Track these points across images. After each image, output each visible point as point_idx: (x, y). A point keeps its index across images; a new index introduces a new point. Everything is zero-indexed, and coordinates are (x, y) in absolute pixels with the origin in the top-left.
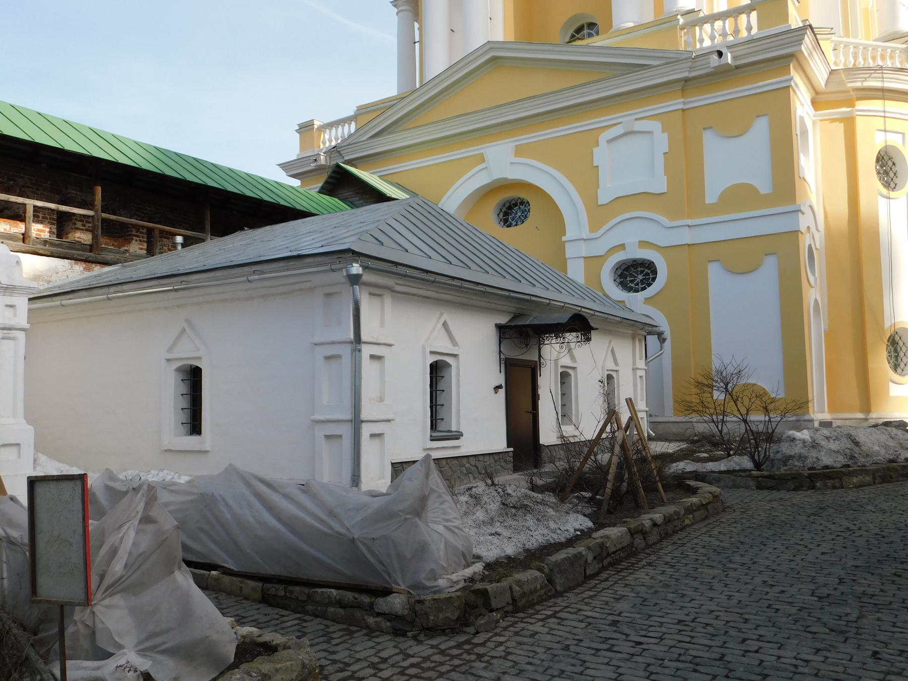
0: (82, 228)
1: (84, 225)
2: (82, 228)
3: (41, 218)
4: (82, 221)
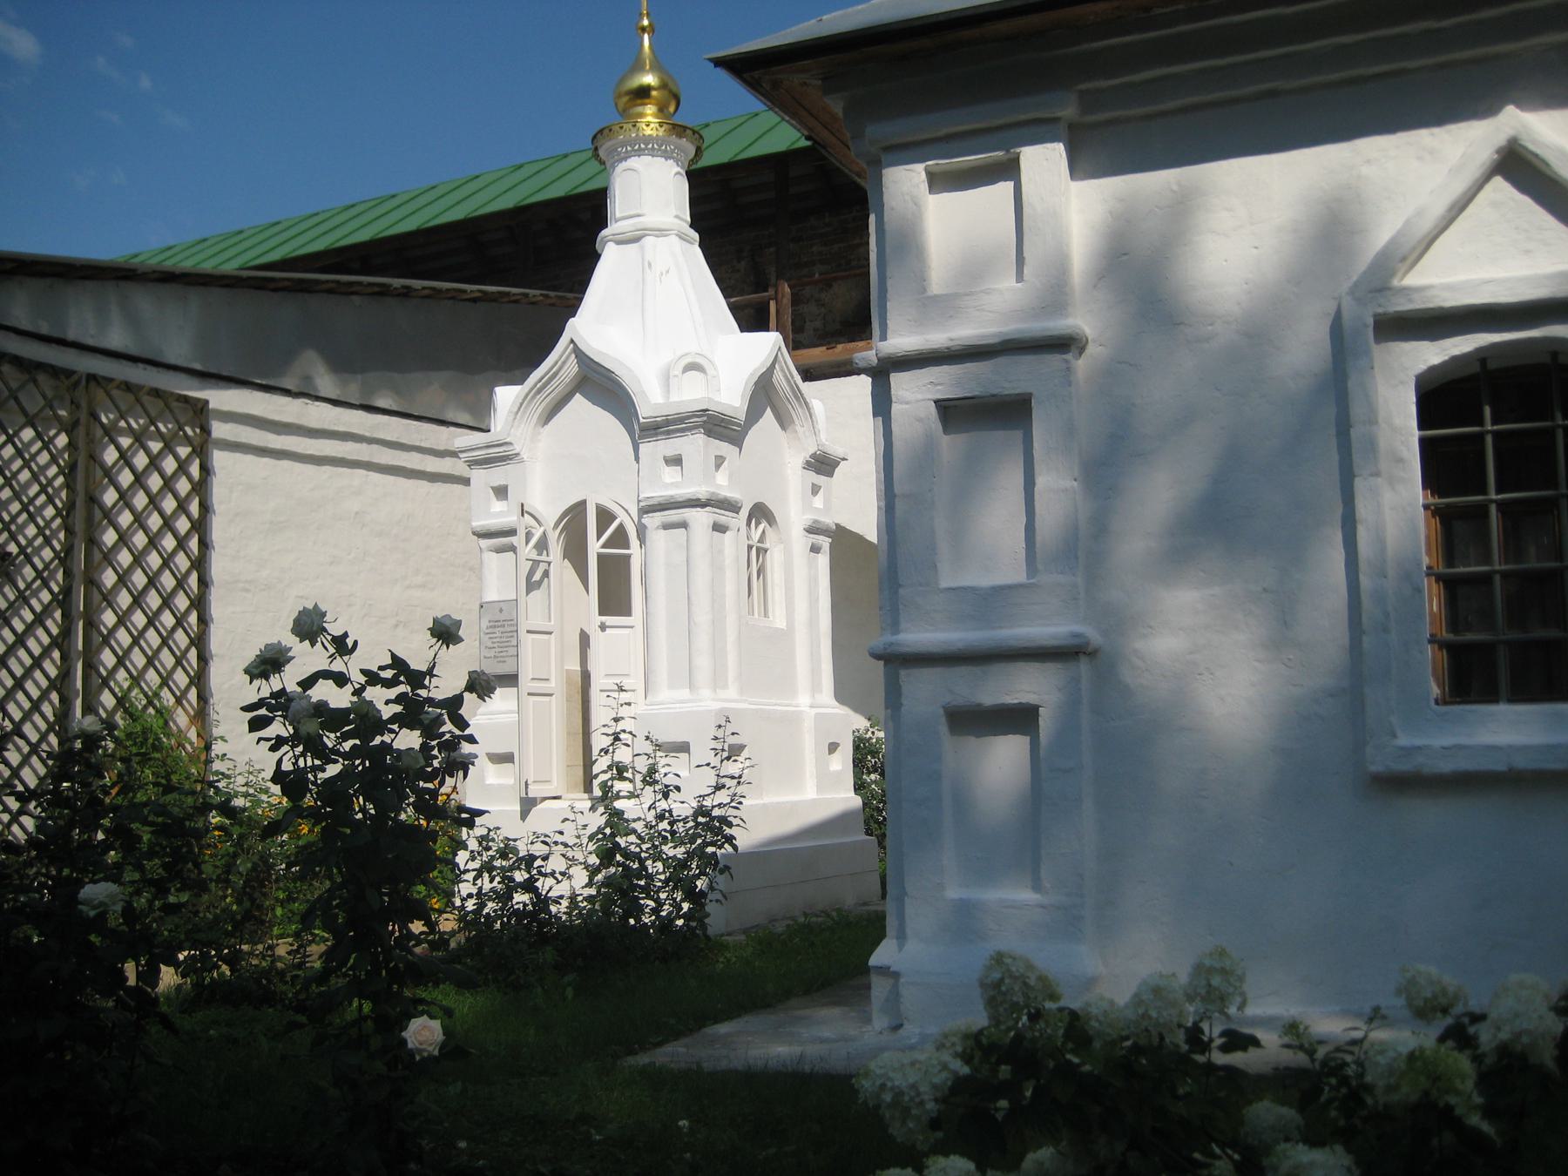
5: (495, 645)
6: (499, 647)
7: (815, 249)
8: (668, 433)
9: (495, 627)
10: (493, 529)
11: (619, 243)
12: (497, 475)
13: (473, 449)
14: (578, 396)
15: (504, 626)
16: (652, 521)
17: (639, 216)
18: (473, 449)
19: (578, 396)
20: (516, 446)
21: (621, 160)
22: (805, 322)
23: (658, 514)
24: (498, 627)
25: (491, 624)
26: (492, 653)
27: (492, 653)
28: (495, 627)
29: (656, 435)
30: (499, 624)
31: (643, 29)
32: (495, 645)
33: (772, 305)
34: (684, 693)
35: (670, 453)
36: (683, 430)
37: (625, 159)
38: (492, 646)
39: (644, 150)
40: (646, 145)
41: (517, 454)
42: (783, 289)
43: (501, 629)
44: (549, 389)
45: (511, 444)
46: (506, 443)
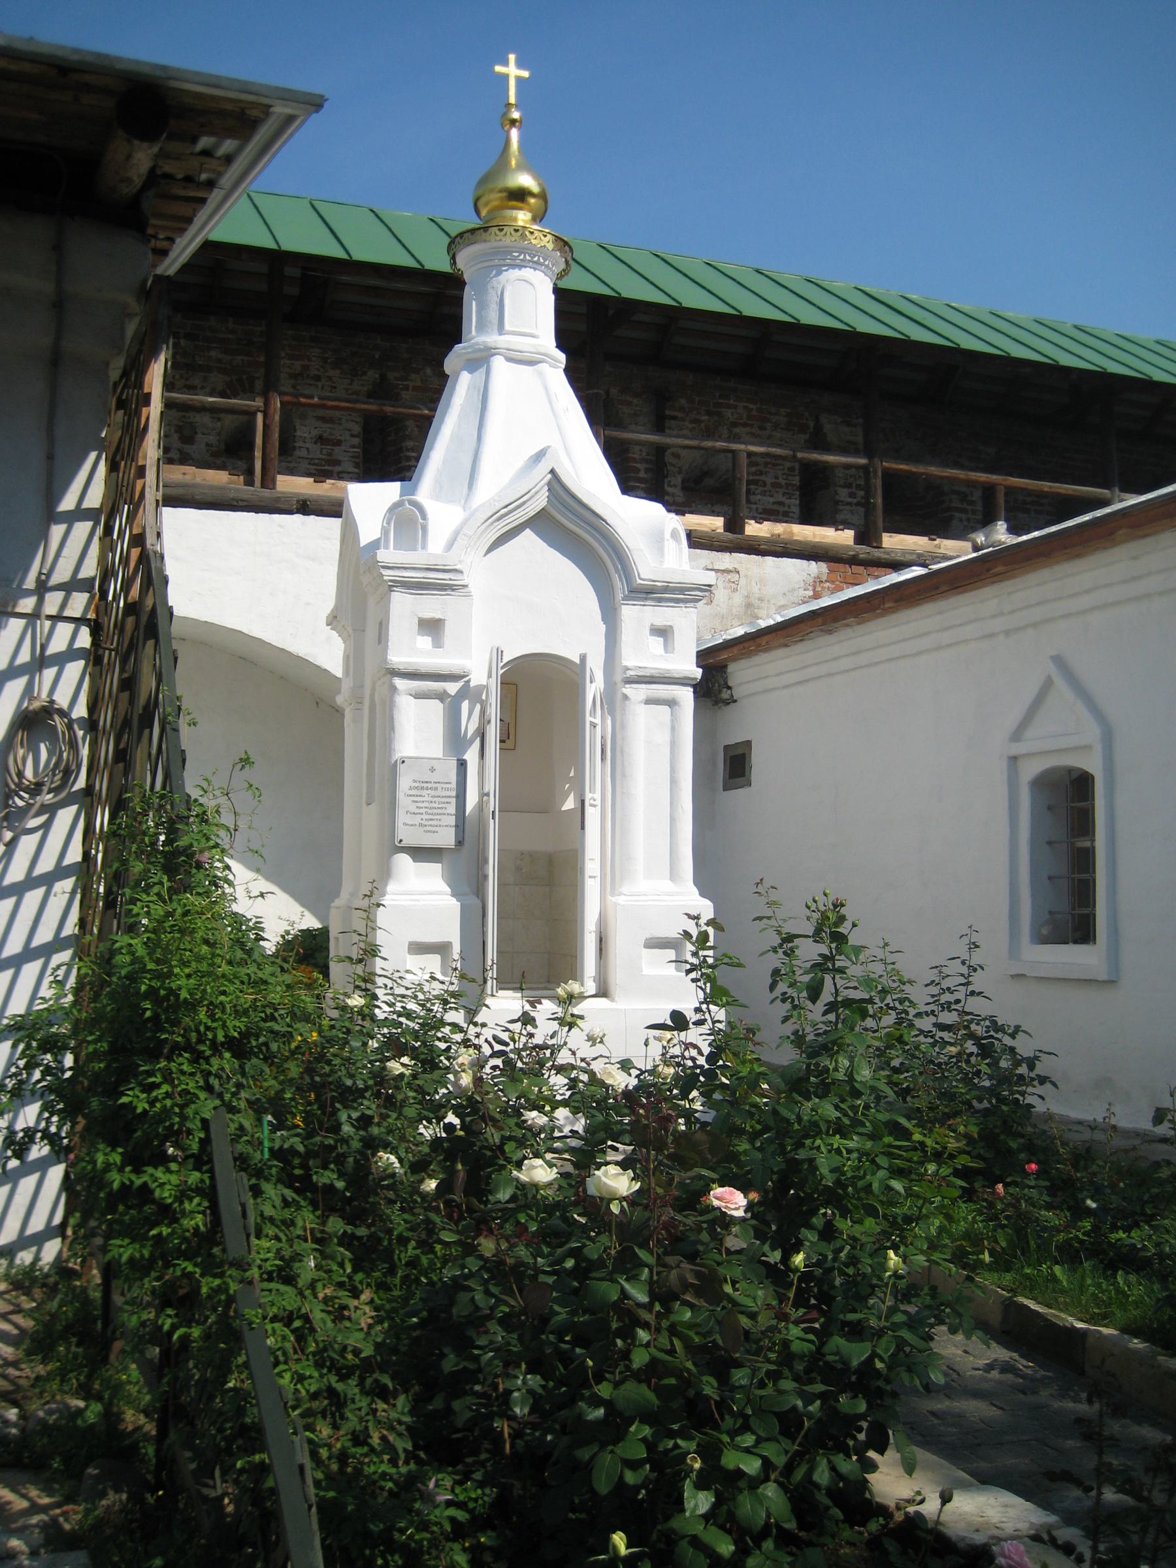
0: (849, 500)
1: (852, 495)
2: (849, 500)
3: (768, 487)
4: (849, 486)
5: (421, 811)
6: (427, 813)
7: (213, 354)
8: (660, 600)
9: (422, 788)
10: (423, 670)
11: (509, 359)
12: (430, 606)
13: (398, 568)
14: (528, 532)
15: (436, 789)
16: (637, 693)
17: (533, 336)
18: (398, 568)
19: (528, 532)
20: (465, 575)
21: (513, 266)
22: (196, 433)
23: (643, 686)
24: (427, 789)
25: (416, 785)
26: (417, 820)
27: (417, 820)
28: (422, 788)
29: (646, 599)
30: (429, 785)
31: (513, 122)
32: (421, 811)
33: (260, 417)
34: (668, 885)
35: (660, 622)
36: (678, 601)
37: (520, 267)
38: (417, 811)
39: (542, 264)
40: (545, 260)
41: (465, 586)
42: (275, 403)
43: (432, 793)
44: (508, 520)
45: (462, 572)
46: (456, 571)
